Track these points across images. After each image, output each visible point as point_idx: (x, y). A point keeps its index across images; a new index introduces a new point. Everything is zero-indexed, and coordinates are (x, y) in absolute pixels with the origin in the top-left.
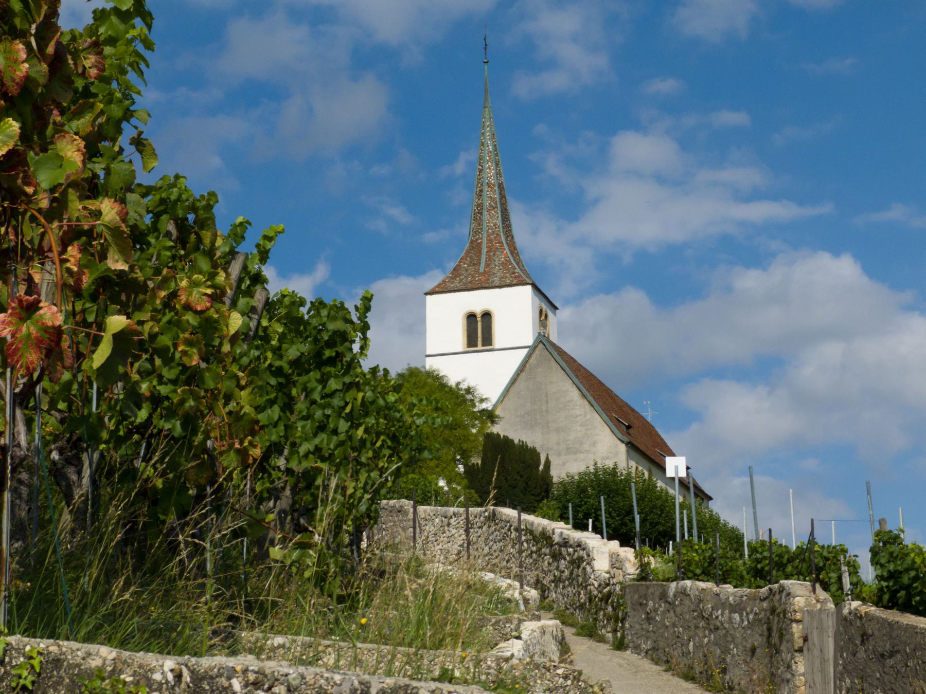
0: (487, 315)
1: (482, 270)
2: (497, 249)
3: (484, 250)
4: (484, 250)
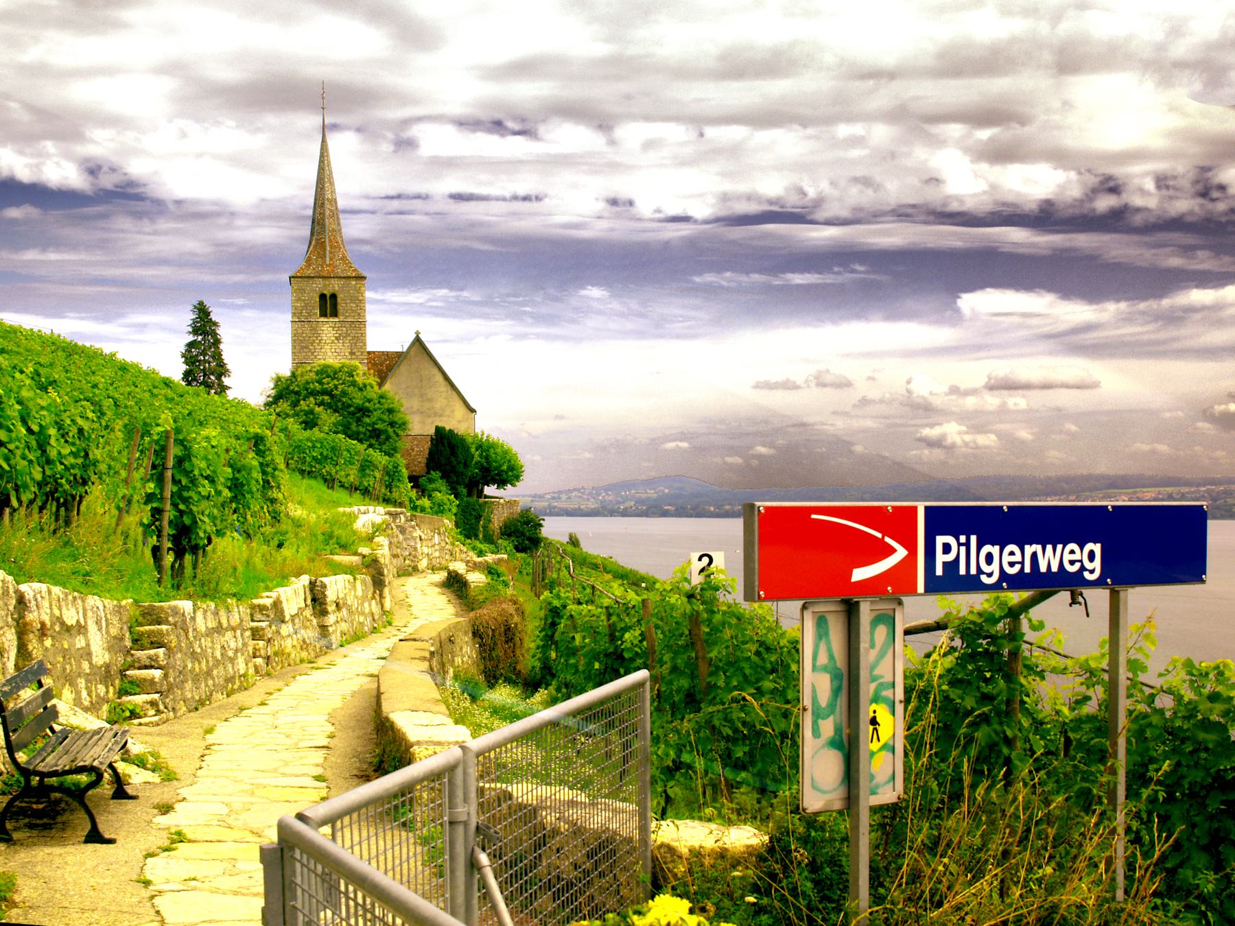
0: (334, 296)
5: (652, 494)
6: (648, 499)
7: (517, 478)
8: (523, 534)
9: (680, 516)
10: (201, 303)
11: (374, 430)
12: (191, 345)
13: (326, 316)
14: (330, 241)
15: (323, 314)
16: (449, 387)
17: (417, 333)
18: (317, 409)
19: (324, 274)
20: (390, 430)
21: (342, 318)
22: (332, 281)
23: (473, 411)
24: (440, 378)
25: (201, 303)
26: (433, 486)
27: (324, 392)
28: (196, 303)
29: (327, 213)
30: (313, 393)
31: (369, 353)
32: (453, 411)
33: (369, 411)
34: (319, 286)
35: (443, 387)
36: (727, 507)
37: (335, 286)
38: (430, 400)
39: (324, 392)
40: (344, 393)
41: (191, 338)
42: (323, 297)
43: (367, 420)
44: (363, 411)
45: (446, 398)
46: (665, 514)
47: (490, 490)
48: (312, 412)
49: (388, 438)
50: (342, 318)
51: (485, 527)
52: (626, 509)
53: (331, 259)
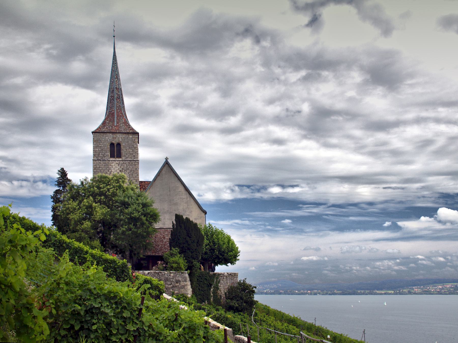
0: (119, 145)
1: (115, 125)
2: (121, 116)
3: (116, 116)
4: (116, 116)
5: (275, 286)
6: (274, 288)
7: (236, 260)
8: (242, 298)
9: (286, 294)
10: (62, 169)
11: (131, 218)
12: (57, 192)
13: (114, 157)
14: (117, 112)
15: (112, 156)
16: (188, 195)
17: (167, 159)
18: (94, 204)
19: (113, 131)
20: (144, 219)
21: (124, 158)
22: (118, 135)
23: (205, 213)
24: (182, 189)
25: (62, 169)
26: (174, 259)
27: (101, 194)
28: (59, 169)
29: (116, 96)
30: (94, 195)
31: (141, 182)
32: (191, 212)
33: (129, 205)
34: (109, 138)
35: (185, 195)
36: (302, 291)
37: (119, 138)
38: (176, 204)
39: (101, 194)
40: (114, 194)
41: (57, 188)
42: (112, 145)
43: (126, 211)
44: (125, 205)
45: (187, 203)
46: (280, 294)
47: (220, 269)
48: (90, 207)
49: (143, 224)
50: (124, 158)
51: (215, 293)
52: (266, 292)
53: (117, 123)
